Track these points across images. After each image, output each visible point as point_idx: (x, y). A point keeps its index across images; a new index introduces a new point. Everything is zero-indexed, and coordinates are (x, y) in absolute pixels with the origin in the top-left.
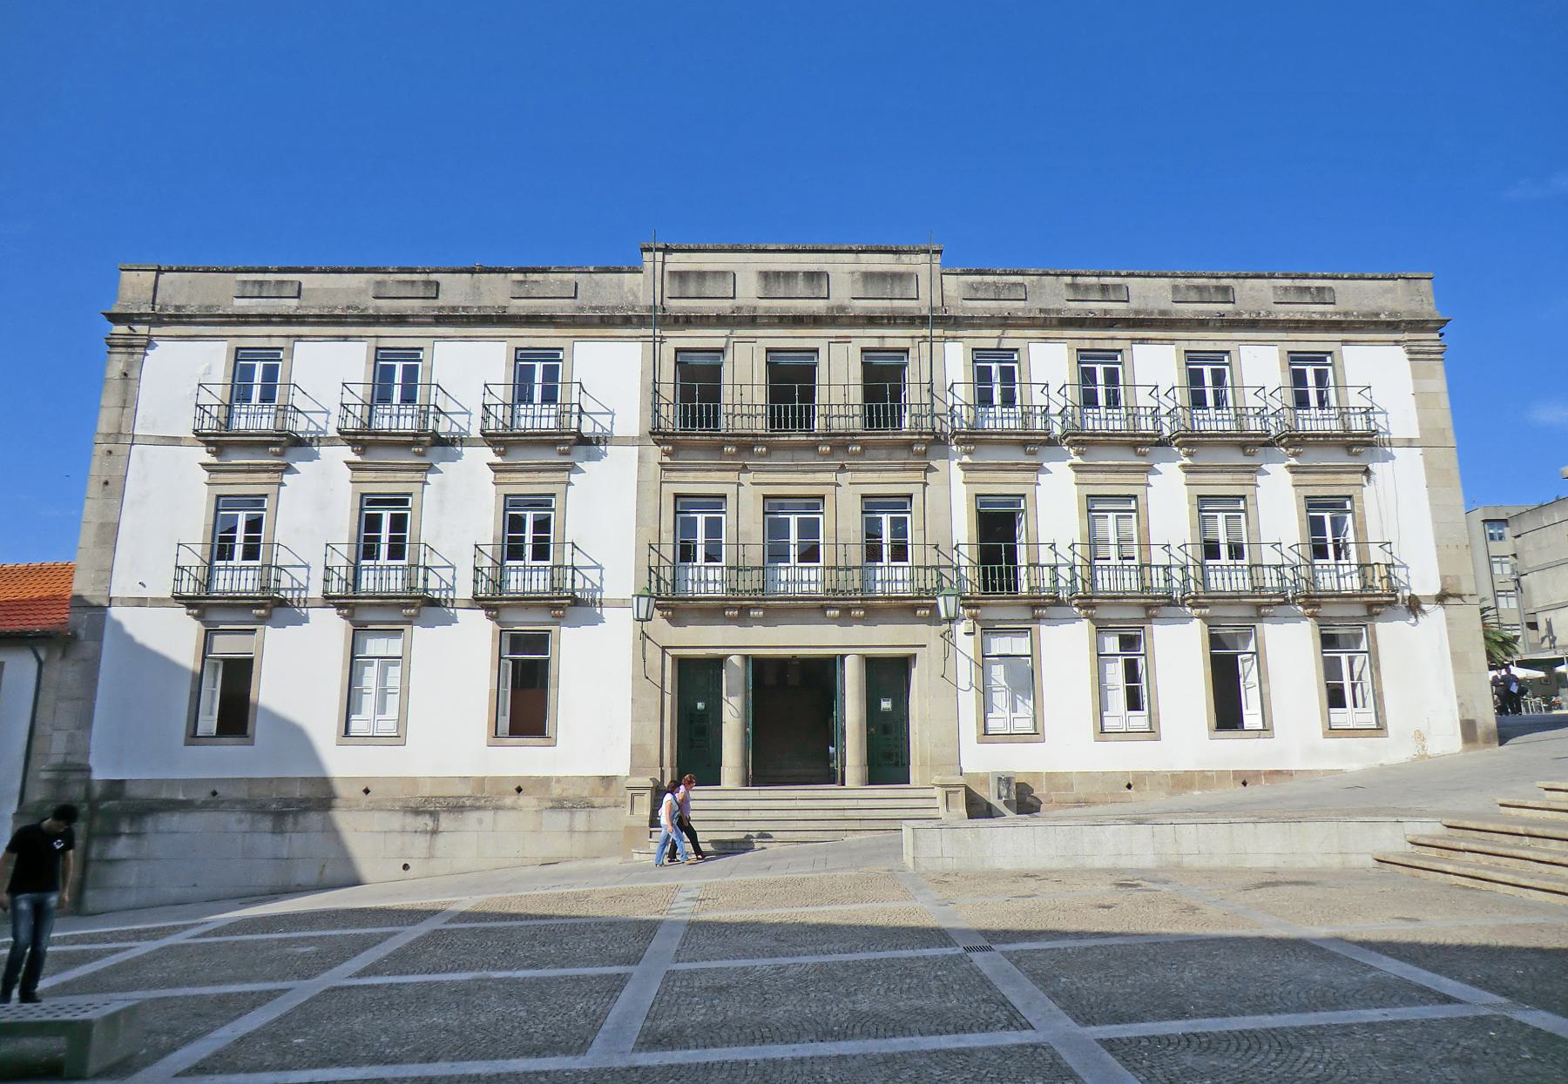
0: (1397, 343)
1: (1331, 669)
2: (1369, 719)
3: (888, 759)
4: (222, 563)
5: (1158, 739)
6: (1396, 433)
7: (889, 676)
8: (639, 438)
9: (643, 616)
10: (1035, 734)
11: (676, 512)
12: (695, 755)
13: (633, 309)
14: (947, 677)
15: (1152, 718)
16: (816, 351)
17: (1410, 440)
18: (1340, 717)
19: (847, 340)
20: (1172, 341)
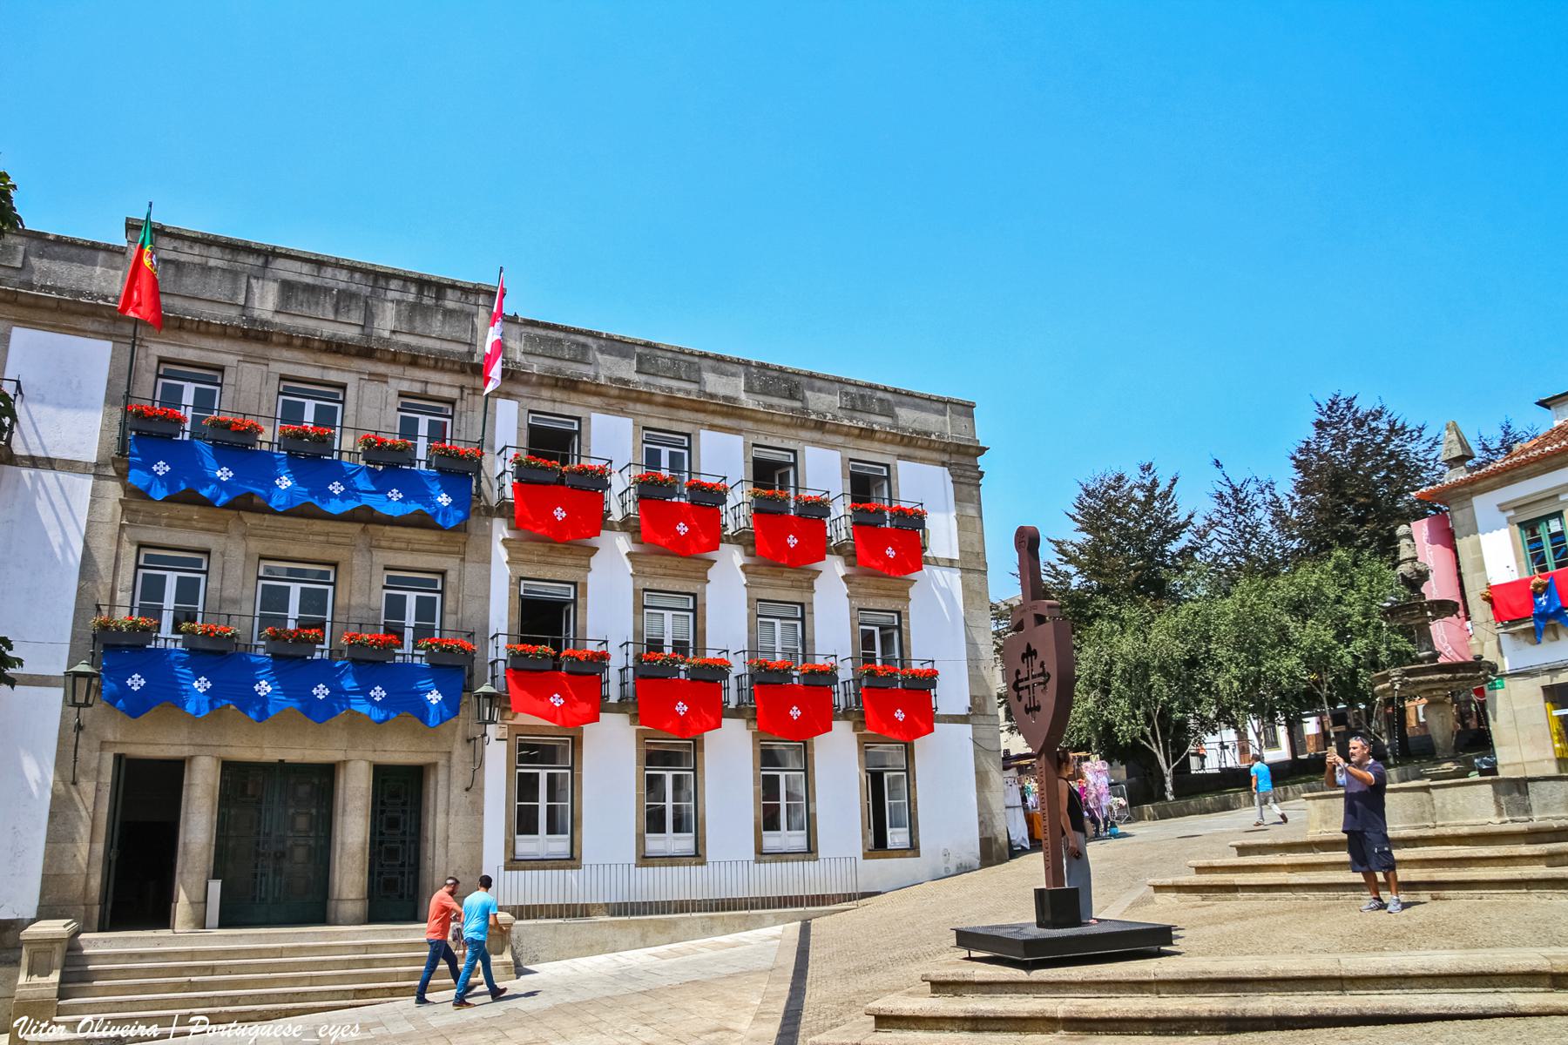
0: (943, 464)
1: (769, 787)
2: (797, 840)
3: (396, 890)
4: (437, 634)
5: (703, 863)
6: (84, 485)
7: (401, 793)
8: (97, 465)
9: (81, 699)
10: (572, 860)
11: (138, 567)
12: (136, 892)
13: (105, 298)
14: (474, 786)
15: (699, 843)
16: (343, 387)
17: (951, 561)
18: (772, 841)
19: (382, 378)
20: (738, 431)
